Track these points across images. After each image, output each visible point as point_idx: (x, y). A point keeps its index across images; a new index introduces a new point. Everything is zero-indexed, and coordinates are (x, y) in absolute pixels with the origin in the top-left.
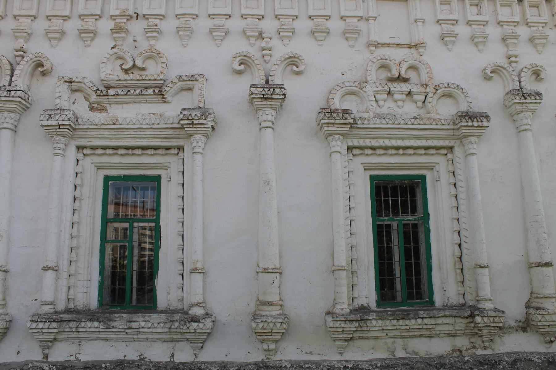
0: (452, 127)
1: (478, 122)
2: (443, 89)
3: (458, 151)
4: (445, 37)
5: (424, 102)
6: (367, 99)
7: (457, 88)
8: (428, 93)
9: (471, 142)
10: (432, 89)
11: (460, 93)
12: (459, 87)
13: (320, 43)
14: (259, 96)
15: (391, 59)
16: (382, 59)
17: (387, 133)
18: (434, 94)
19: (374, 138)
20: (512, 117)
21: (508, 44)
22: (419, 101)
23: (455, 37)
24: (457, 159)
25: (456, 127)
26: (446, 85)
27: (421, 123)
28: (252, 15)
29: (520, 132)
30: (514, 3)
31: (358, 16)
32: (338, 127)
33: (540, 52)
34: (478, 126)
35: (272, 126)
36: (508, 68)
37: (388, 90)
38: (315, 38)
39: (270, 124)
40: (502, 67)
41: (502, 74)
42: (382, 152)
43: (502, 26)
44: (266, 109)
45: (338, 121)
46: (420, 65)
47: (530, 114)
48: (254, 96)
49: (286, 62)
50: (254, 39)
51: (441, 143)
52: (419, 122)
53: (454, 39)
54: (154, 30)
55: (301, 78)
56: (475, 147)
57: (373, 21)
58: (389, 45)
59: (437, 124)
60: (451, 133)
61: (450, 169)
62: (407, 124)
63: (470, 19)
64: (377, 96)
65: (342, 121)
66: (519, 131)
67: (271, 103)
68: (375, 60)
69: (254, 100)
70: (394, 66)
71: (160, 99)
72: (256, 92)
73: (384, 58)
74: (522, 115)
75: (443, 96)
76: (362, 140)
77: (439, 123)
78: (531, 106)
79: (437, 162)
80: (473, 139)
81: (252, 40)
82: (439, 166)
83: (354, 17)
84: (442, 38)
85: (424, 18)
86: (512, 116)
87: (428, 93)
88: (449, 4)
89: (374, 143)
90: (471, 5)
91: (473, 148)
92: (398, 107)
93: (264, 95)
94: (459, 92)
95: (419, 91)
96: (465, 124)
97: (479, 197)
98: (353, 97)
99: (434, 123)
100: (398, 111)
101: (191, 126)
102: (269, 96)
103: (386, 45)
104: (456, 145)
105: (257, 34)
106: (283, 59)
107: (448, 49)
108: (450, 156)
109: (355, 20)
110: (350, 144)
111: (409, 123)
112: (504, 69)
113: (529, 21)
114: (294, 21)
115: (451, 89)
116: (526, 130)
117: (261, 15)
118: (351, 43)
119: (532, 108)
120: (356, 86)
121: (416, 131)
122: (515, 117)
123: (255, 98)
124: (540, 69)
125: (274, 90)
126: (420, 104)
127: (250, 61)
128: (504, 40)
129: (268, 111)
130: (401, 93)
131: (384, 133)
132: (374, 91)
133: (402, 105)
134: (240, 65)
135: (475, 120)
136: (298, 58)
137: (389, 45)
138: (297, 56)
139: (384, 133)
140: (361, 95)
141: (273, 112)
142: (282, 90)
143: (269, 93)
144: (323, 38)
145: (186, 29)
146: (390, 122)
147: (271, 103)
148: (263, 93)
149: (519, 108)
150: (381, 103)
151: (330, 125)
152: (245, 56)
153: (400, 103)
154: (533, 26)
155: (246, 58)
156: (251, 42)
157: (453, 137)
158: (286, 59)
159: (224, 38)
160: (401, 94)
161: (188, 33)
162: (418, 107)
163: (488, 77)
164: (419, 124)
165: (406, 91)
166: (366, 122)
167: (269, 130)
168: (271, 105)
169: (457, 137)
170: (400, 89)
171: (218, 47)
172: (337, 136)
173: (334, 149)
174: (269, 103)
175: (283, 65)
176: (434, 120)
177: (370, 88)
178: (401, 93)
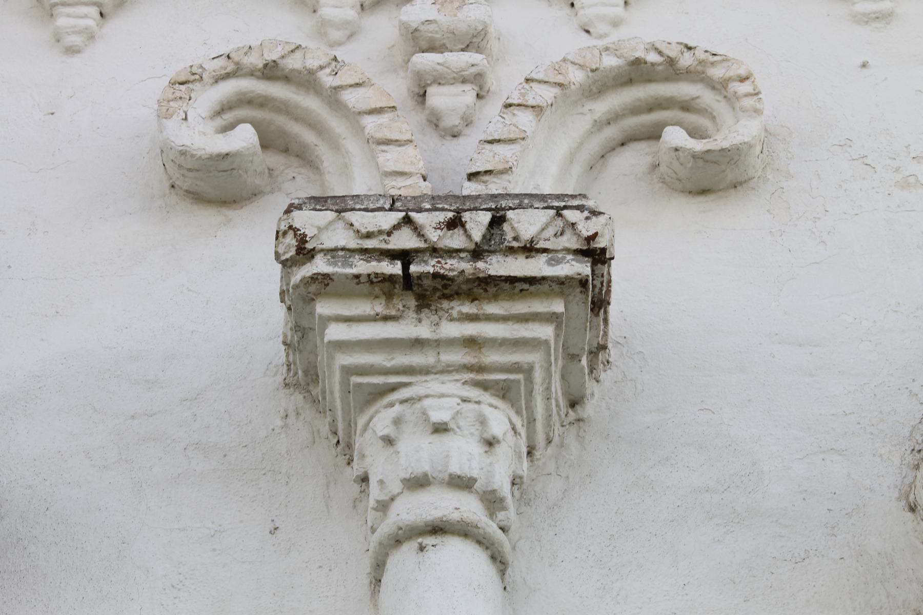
14: (362, 267)
35: (491, 527)
39: (466, 507)
44: (433, 385)
48: (320, 265)
49: (602, 107)
69: (323, 308)
72: (341, 238)
93: (405, 257)
102: (453, 266)
106: (576, 76)
123: (323, 280)
125: (497, 221)
127: (310, 103)
129: (444, 396)
134: (230, 127)
136: (694, 75)
138: (686, 60)
141: (499, 418)
142: (571, 215)
143: (456, 240)
148: (405, 240)
152: (271, 72)
155: (277, 90)
158: (601, 84)
167: (457, 555)
168: (471, 343)
171: (72, 51)
175: (580, 123)
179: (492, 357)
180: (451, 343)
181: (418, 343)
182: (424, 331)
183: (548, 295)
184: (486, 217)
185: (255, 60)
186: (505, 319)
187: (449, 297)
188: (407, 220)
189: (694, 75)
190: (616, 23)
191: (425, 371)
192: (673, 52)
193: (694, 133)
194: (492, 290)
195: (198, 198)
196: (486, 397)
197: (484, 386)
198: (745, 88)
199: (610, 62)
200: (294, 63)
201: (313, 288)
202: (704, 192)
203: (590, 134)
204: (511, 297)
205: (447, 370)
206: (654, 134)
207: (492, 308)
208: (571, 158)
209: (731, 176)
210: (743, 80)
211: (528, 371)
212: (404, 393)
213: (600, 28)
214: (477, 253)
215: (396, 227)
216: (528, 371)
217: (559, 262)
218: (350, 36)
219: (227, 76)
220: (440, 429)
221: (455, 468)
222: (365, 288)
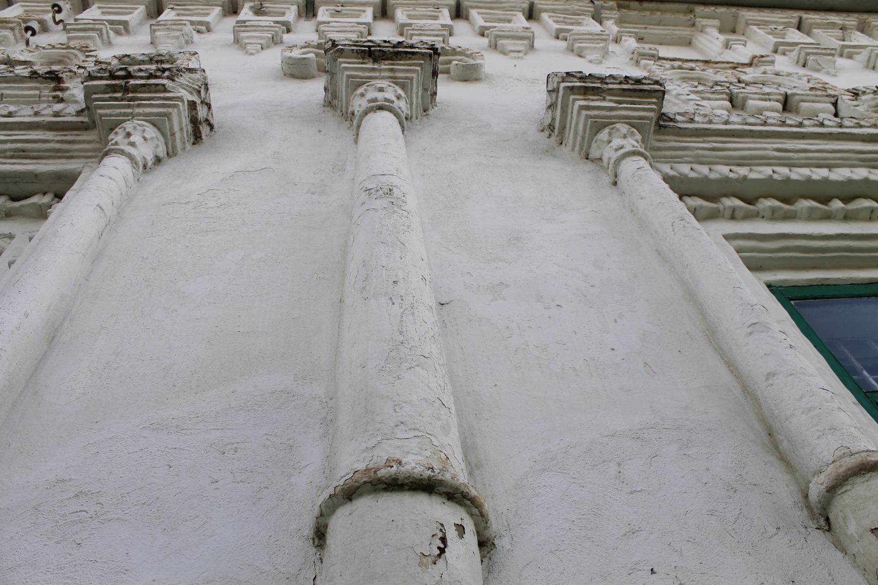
6: (677, 101)
17: (775, 146)
38: (504, 53)
54: (91, 26)
71: (46, 92)
101: (119, 95)
136: (460, 54)
145: (174, 27)
159: (268, 47)
160: (765, 100)
161: (178, 34)
168: (392, 70)
180: (385, 70)
181: (373, 70)
186: (404, 65)
191: (376, 78)
194: (399, 57)
195: (293, 76)
197: (396, 84)
201: (337, 54)
202: (466, 81)
205: (383, 78)
211: (411, 79)
216: (411, 79)
219: (305, 47)
222: (355, 54)
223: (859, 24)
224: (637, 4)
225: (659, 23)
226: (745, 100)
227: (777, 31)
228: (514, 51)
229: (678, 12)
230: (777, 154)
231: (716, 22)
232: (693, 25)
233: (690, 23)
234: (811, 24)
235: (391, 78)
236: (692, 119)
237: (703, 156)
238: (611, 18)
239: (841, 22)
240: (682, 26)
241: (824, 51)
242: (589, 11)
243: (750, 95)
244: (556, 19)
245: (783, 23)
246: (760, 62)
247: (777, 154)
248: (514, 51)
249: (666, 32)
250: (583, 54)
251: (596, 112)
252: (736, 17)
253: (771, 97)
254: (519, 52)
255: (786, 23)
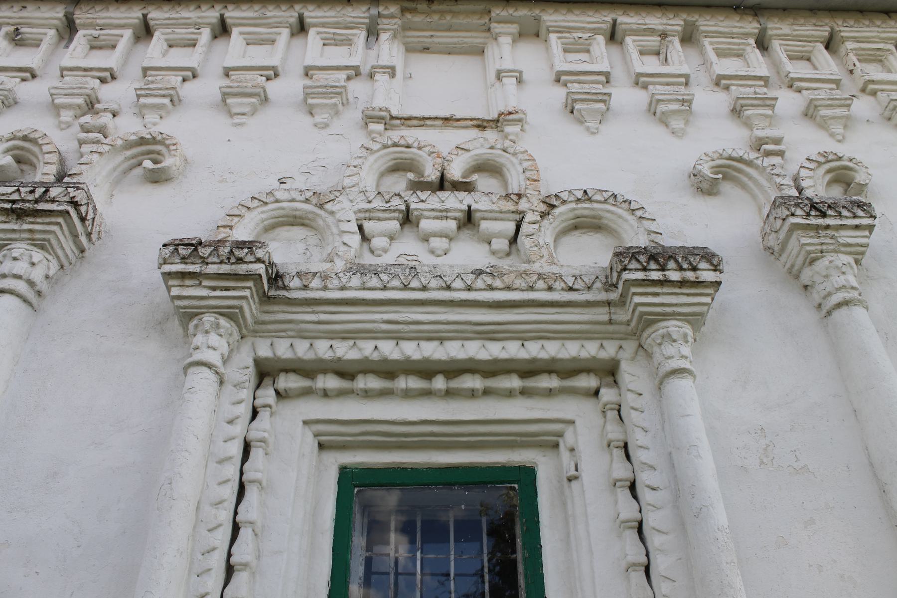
0: (603, 296)
1: (681, 269)
2: (573, 205)
3: (632, 374)
4: (575, 101)
5: (514, 240)
7: (611, 200)
8: (522, 213)
9: (668, 337)
10: (536, 202)
11: (626, 215)
12: (620, 199)
13: (237, 119)
15: (422, 144)
16: (395, 145)
17: (386, 317)
18: (543, 215)
19: (344, 336)
20: (798, 279)
21: (748, 117)
22: (499, 235)
23: (604, 101)
24: (630, 396)
25: (614, 296)
26: (580, 194)
27: (498, 283)
28: (85, 70)
29: (829, 313)
30: (749, 49)
31: (347, 68)
32: (214, 289)
33: (840, 138)
34: (683, 283)
36: (759, 162)
37: (403, 207)
40: (740, 160)
41: (745, 179)
42: (373, 383)
43: (727, 88)
45: (212, 269)
46: (504, 159)
47: (850, 259)
49: (129, 153)
50: (71, 113)
51: (571, 350)
52: (489, 280)
53: (601, 106)
55: (162, 192)
56: (686, 350)
57: (386, 77)
58: (423, 121)
59: (550, 289)
60: (601, 314)
61: (611, 436)
62: (448, 288)
63: (640, 70)
64: (368, 226)
65: (225, 268)
66: (827, 311)
67: (31, 227)
68: (376, 146)
70: (429, 158)
73: (402, 142)
74: (822, 265)
75: (576, 227)
76: (306, 344)
77: (558, 285)
78: (846, 236)
79: (569, 417)
80: (673, 326)
81: (67, 116)
82: (575, 432)
83: (338, 68)
84: (569, 108)
85: (519, 67)
86: (797, 277)
87: (522, 213)
88: (588, 51)
89: (345, 351)
90: (642, 53)
91: (678, 353)
92: (432, 252)
93: (14, 202)
94: (620, 211)
95: (495, 207)
96: (640, 275)
97: (720, 516)
98: (298, 232)
99: (541, 284)
100: (427, 259)
102: (28, 205)
103: (415, 122)
104: (625, 358)
105: (80, 101)
107: (588, 129)
108: (608, 395)
109: (343, 75)
110: (264, 351)
111: (458, 284)
112: (749, 163)
113: (791, 75)
114: (187, 84)
115: (596, 205)
116: (846, 303)
117: (105, 70)
118: (318, 119)
119: (850, 241)
120: (307, 201)
121: (484, 310)
122: (806, 275)
124: (851, 164)
126: (501, 244)
127: (35, 149)
128: (736, 112)
129: (19, 248)
130: (443, 214)
131: (377, 317)
132: (360, 211)
133: (447, 246)
135: (671, 264)
136: (161, 143)
137: (423, 121)
138: (159, 138)
139: (377, 317)
140: (321, 222)
144: (246, 110)
146: (396, 283)
147: (31, 227)
148: (15, 197)
149: (809, 241)
150: (378, 242)
151: (188, 282)
152: (25, 138)
153: (438, 243)
154: (807, 89)
156: (62, 118)
157: (611, 328)
160: (441, 218)
162: (494, 253)
163: (705, 186)
164: (491, 288)
165: (455, 210)
166: (316, 283)
168: (30, 231)
169: (623, 328)
170: (438, 206)
172: (208, 319)
173: (197, 356)
174: (26, 227)
175: (120, 158)
176: (541, 276)
177: (346, 204)
178: (443, 214)
179: (37, 236)
181: (14, 231)
182: (16, 227)
183: (57, 216)
184: (44, 189)
185: (20, 134)
187: (27, 216)
188: (18, 190)
189: (161, 143)
190: (155, 124)
191: (16, 240)
192: (721, 152)
193: (155, 162)
196: (36, 249)
197: (35, 245)
198: (174, 148)
199: (133, 137)
200: (32, 136)
202: (156, 182)
203: (123, 162)
204: (46, 216)
206: (140, 164)
207: (39, 220)
208: (114, 169)
209: (164, 177)
210: (174, 145)
212: (9, 247)
213: (148, 126)
214: (37, 201)
215: (13, 192)
217: (60, 205)
218: (69, 126)
219: (11, 140)
220: (15, 259)
221: (15, 272)
223: (684, 30)
224: (423, 6)
225: (449, 29)
226: (418, 219)
227: (581, 41)
228: (238, 114)
229: (474, 13)
230: (385, 327)
231: (514, 28)
232: (489, 30)
233: (484, 28)
234: (625, 30)
235: (30, 239)
236: (306, 286)
237: (306, 331)
238: (389, 30)
239: (661, 28)
240: (476, 30)
241: (594, 97)
242: (363, 23)
243: (426, 213)
244: (324, 36)
245: (590, 30)
246: (506, 120)
247: (385, 327)
248: (238, 114)
249: (456, 40)
250: (313, 112)
251: (185, 303)
252: (538, 20)
253: (449, 214)
254: (243, 114)
255: (594, 29)
